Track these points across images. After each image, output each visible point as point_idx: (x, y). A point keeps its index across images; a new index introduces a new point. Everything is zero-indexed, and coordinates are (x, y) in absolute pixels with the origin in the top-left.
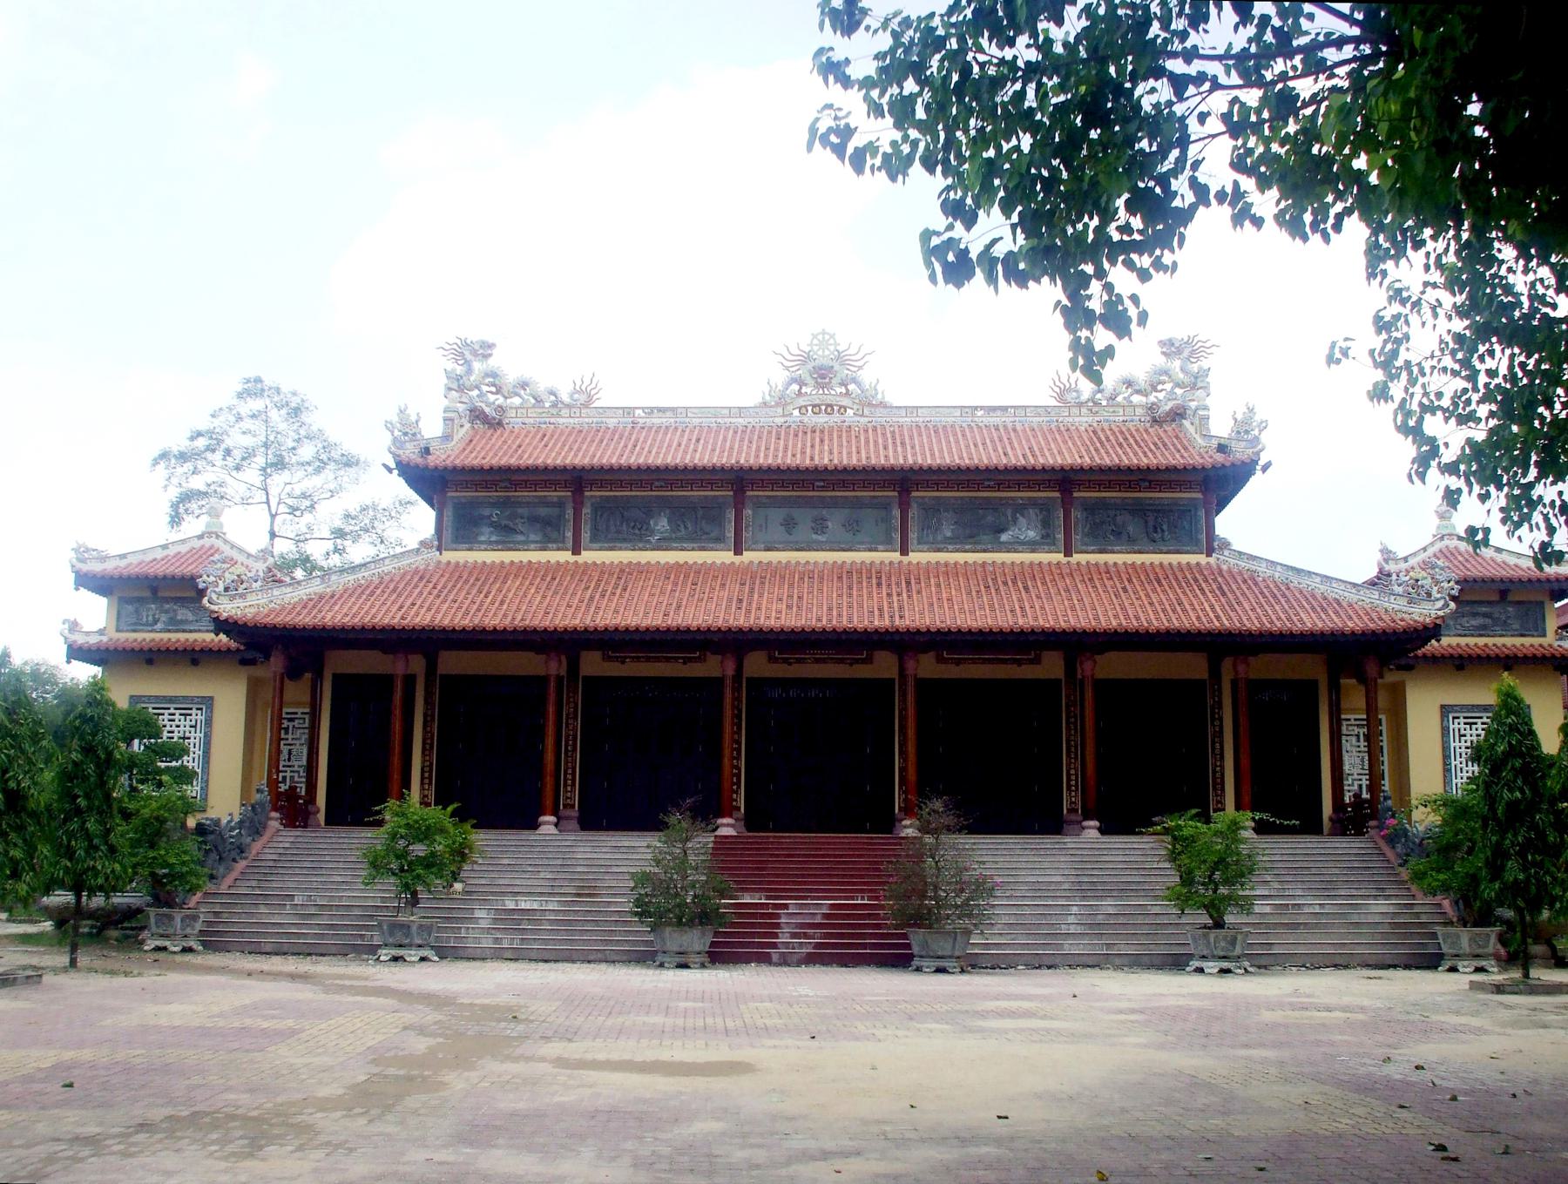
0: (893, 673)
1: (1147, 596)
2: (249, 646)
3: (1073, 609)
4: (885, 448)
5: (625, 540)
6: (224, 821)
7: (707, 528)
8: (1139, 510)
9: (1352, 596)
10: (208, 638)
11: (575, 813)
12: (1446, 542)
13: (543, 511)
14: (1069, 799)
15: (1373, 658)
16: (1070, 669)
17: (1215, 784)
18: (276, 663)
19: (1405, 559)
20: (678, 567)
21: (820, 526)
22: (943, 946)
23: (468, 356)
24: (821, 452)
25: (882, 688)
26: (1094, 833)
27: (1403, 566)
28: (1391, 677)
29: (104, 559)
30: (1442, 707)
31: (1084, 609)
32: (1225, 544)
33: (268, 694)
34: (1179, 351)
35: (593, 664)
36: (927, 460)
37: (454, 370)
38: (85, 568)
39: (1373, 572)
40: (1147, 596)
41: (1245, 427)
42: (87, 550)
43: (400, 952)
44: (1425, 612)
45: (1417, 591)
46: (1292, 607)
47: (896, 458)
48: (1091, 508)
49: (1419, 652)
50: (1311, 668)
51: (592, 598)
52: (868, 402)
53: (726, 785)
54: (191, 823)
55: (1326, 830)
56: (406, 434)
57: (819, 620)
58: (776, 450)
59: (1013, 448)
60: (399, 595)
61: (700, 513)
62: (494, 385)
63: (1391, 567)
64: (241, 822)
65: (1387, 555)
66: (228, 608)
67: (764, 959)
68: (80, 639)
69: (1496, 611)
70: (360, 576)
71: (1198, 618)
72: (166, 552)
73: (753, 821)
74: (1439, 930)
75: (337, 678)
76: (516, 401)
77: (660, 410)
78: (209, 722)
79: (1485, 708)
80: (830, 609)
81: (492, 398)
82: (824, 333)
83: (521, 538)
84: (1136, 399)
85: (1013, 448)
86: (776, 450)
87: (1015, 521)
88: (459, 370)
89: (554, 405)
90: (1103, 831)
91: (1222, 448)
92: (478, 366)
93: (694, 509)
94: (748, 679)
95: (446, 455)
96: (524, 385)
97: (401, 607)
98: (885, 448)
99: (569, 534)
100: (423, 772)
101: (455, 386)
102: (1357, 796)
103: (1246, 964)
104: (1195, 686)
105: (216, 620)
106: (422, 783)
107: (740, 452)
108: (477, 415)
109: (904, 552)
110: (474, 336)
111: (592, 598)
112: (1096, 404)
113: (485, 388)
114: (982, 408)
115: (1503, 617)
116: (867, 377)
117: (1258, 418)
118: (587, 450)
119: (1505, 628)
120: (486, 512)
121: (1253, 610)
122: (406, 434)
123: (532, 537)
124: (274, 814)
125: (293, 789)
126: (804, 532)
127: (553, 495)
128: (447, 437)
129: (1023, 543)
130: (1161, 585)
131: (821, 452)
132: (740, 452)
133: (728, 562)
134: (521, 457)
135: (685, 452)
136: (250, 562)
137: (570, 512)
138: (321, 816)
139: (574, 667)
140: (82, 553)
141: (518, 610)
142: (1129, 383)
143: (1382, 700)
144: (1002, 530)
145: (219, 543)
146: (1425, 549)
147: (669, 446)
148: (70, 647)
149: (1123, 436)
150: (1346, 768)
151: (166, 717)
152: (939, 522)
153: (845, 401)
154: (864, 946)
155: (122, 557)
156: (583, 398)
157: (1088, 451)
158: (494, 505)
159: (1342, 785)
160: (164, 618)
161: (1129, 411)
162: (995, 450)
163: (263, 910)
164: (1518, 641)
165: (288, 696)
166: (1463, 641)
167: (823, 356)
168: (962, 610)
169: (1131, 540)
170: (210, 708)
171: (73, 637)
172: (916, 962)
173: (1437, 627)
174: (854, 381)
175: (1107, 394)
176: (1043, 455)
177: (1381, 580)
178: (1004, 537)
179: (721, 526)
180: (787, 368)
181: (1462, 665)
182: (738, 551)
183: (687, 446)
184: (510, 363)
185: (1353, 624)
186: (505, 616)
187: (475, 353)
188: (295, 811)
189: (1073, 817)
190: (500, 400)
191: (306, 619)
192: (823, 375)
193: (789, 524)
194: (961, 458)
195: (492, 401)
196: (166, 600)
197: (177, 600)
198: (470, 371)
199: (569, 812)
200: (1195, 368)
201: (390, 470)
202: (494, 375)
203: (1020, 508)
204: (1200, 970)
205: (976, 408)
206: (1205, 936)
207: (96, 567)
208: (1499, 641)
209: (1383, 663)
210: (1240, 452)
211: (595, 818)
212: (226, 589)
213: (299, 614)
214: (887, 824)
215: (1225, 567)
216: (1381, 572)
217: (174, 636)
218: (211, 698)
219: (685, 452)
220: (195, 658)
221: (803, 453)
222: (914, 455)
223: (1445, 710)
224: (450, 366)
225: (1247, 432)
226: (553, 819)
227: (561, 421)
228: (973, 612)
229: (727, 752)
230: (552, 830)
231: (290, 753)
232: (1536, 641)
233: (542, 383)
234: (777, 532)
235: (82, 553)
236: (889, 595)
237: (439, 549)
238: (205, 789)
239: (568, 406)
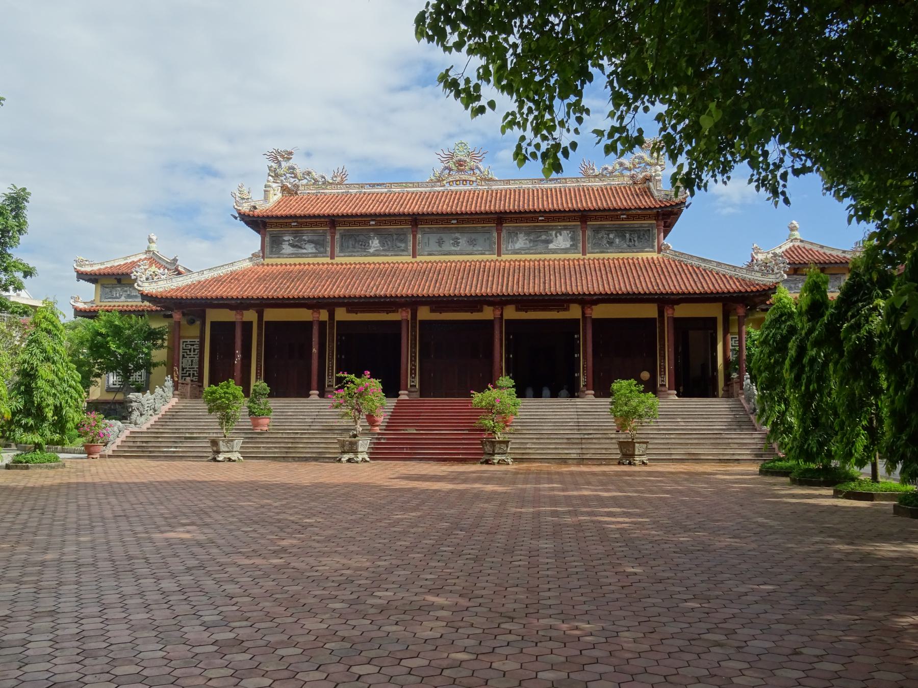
7: (399, 244)
16: (661, 313)
23: (280, 159)
25: (488, 325)
38: (82, 269)
44: (769, 280)
50: (714, 311)
55: (721, 392)
61: (395, 237)
62: (293, 173)
68: (81, 306)
76: (305, 182)
81: (292, 180)
87: (556, 236)
89: (324, 183)
94: (212, 323)
96: (309, 173)
99: (329, 249)
104: (650, 322)
113: (288, 175)
137: (329, 237)
139: (332, 315)
140: (80, 263)
154: (459, 454)
156: (339, 179)
160: (124, 294)
174: (478, 168)
177: (750, 267)
178: (551, 246)
180: (442, 162)
184: (299, 164)
187: (282, 156)
189: (663, 389)
193: (440, 243)
199: (413, 389)
201: (236, 218)
207: (88, 269)
212: (147, 279)
226: (406, 392)
230: (317, 398)
234: (434, 247)
237: (263, 257)
239: (331, 184)
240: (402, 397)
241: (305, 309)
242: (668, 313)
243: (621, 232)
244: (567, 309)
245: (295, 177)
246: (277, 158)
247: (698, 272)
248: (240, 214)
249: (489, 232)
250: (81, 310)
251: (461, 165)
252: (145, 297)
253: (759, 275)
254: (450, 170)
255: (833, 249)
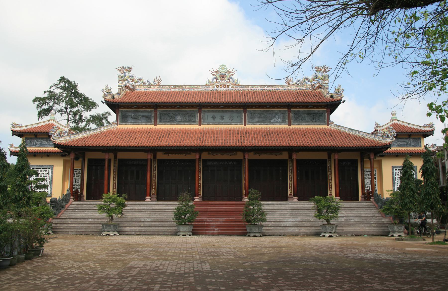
0: (242, 158)
1: (311, 137)
2: (64, 151)
3: (290, 140)
4: (240, 97)
5: (169, 122)
6: (58, 199)
8: (309, 113)
9: (366, 137)
10: (53, 149)
11: (155, 196)
12: (394, 122)
13: (146, 114)
14: (290, 191)
15: (373, 152)
16: (290, 157)
17: (329, 187)
18: (72, 156)
19: (382, 126)
20: (307, 131)
21: (222, 118)
22: (255, 229)
24: (222, 98)
26: (296, 200)
27: (382, 128)
28: (378, 159)
29: (20, 127)
30: (392, 166)
31: (293, 140)
32: (333, 123)
33: (69, 165)
34: (321, 70)
35: (160, 156)
36: (252, 100)
37: (120, 75)
38: (15, 129)
39: (373, 130)
40: (311, 137)
41: (338, 92)
42: (15, 124)
43: (108, 233)
44: (387, 141)
45: (385, 136)
46: (350, 139)
47: (243, 99)
48: (296, 113)
49: (386, 152)
51: (160, 138)
52: (236, 84)
53: (197, 188)
54: (48, 200)
55: (360, 198)
56: (107, 93)
57: (222, 143)
58: (210, 97)
59: (275, 97)
60: (107, 137)
63: (378, 129)
64: (62, 199)
65: (377, 125)
66: (58, 141)
67: (206, 234)
68: (14, 149)
69: (407, 140)
70: (95, 132)
71: (325, 142)
72: (38, 125)
73: (203, 198)
74: (389, 226)
75: (89, 160)
76: (138, 84)
77: (178, 86)
78: (52, 172)
79: (398, 167)
80: (225, 140)
81: (131, 83)
82: (223, 65)
83: (140, 121)
84: (309, 83)
85: (275, 97)
86: (210, 97)
88: (123, 75)
89: (149, 85)
90: (299, 200)
91: (332, 97)
92: (127, 74)
93: (188, 113)
95: (118, 98)
96: (140, 79)
97: (107, 140)
98: (240, 97)
100: (113, 185)
101: (121, 79)
102: (368, 190)
103: (336, 234)
105: (55, 144)
106: (113, 188)
107: (200, 98)
108: (126, 87)
109: (245, 125)
110: (126, 65)
111: (160, 138)
112: (298, 84)
113: (129, 80)
114: (266, 86)
115: (409, 142)
116: (235, 77)
117: (341, 89)
118: (158, 97)
119: (410, 145)
120: (130, 114)
121: (340, 140)
122: (107, 93)
123: (143, 121)
124: (72, 197)
125: (77, 190)
126: (218, 119)
127: (149, 110)
128: (119, 94)
129: (277, 122)
130: (315, 134)
131: (222, 98)
132: (200, 98)
133: (197, 128)
134: (140, 99)
135: (185, 98)
136: (64, 128)
137: (153, 115)
138: (85, 198)
139: (155, 157)
140: (14, 125)
141: (140, 141)
142: (307, 79)
143: (375, 165)
144: (272, 119)
145: (54, 123)
146: (388, 124)
147: (181, 96)
148: (11, 152)
149: (305, 94)
150: (366, 183)
151: (40, 171)
152: (254, 117)
153: (229, 84)
154: (234, 230)
155: (26, 126)
156: (156, 83)
157: (295, 98)
158: (132, 112)
159: (364, 188)
161: (306, 86)
162: (270, 97)
163: (69, 222)
164: (413, 149)
165: (75, 166)
166: (398, 149)
167: (223, 72)
168: (260, 141)
169: (306, 121)
170: (53, 168)
171: (11, 149)
172: (248, 234)
173: (390, 144)
174: (231, 78)
175: (301, 82)
176: (283, 99)
177: (375, 133)
178: (272, 121)
179: (195, 118)
180: (213, 75)
181: (397, 155)
182: (200, 125)
183: (186, 96)
184: (135, 74)
185: (367, 144)
186: (136, 142)
188: (77, 196)
189: (291, 196)
190: (134, 84)
191: (80, 144)
192: (223, 76)
193: (214, 118)
194: (260, 99)
195: (130, 84)
196: (39, 139)
197: (42, 139)
198: (125, 76)
199: (153, 196)
200: (324, 75)
201: (103, 103)
202: (132, 76)
203: (277, 113)
204: (324, 236)
205: (265, 86)
206: (325, 227)
207: (18, 129)
208: (408, 149)
209: (376, 155)
210: (337, 97)
211: (160, 197)
212: (57, 135)
213: (78, 142)
214: (241, 199)
215: (332, 129)
216: (375, 130)
217: (42, 149)
218: (53, 166)
219: (185, 98)
220: (48, 155)
221: (217, 98)
222: (248, 99)
223: (393, 167)
224: (120, 74)
225: (339, 92)
226: (149, 197)
227: (151, 89)
228: (263, 141)
229: (197, 179)
230: (149, 200)
231: (76, 180)
232: (419, 149)
233: (145, 79)
234: (210, 119)
235: (14, 125)
236: (241, 137)
237: (117, 124)
238: (51, 191)
239: (153, 85)
240: (196, 200)
241: (101, 153)
242: (295, 156)
243: (184, 114)
244: (281, 154)
245: (133, 81)
246: (123, 71)
247: (347, 136)
248: (105, 101)
249: (240, 112)
250: (14, 152)
251: (223, 77)
252: (56, 145)
253: (381, 138)
254: (217, 79)
255: (414, 125)
